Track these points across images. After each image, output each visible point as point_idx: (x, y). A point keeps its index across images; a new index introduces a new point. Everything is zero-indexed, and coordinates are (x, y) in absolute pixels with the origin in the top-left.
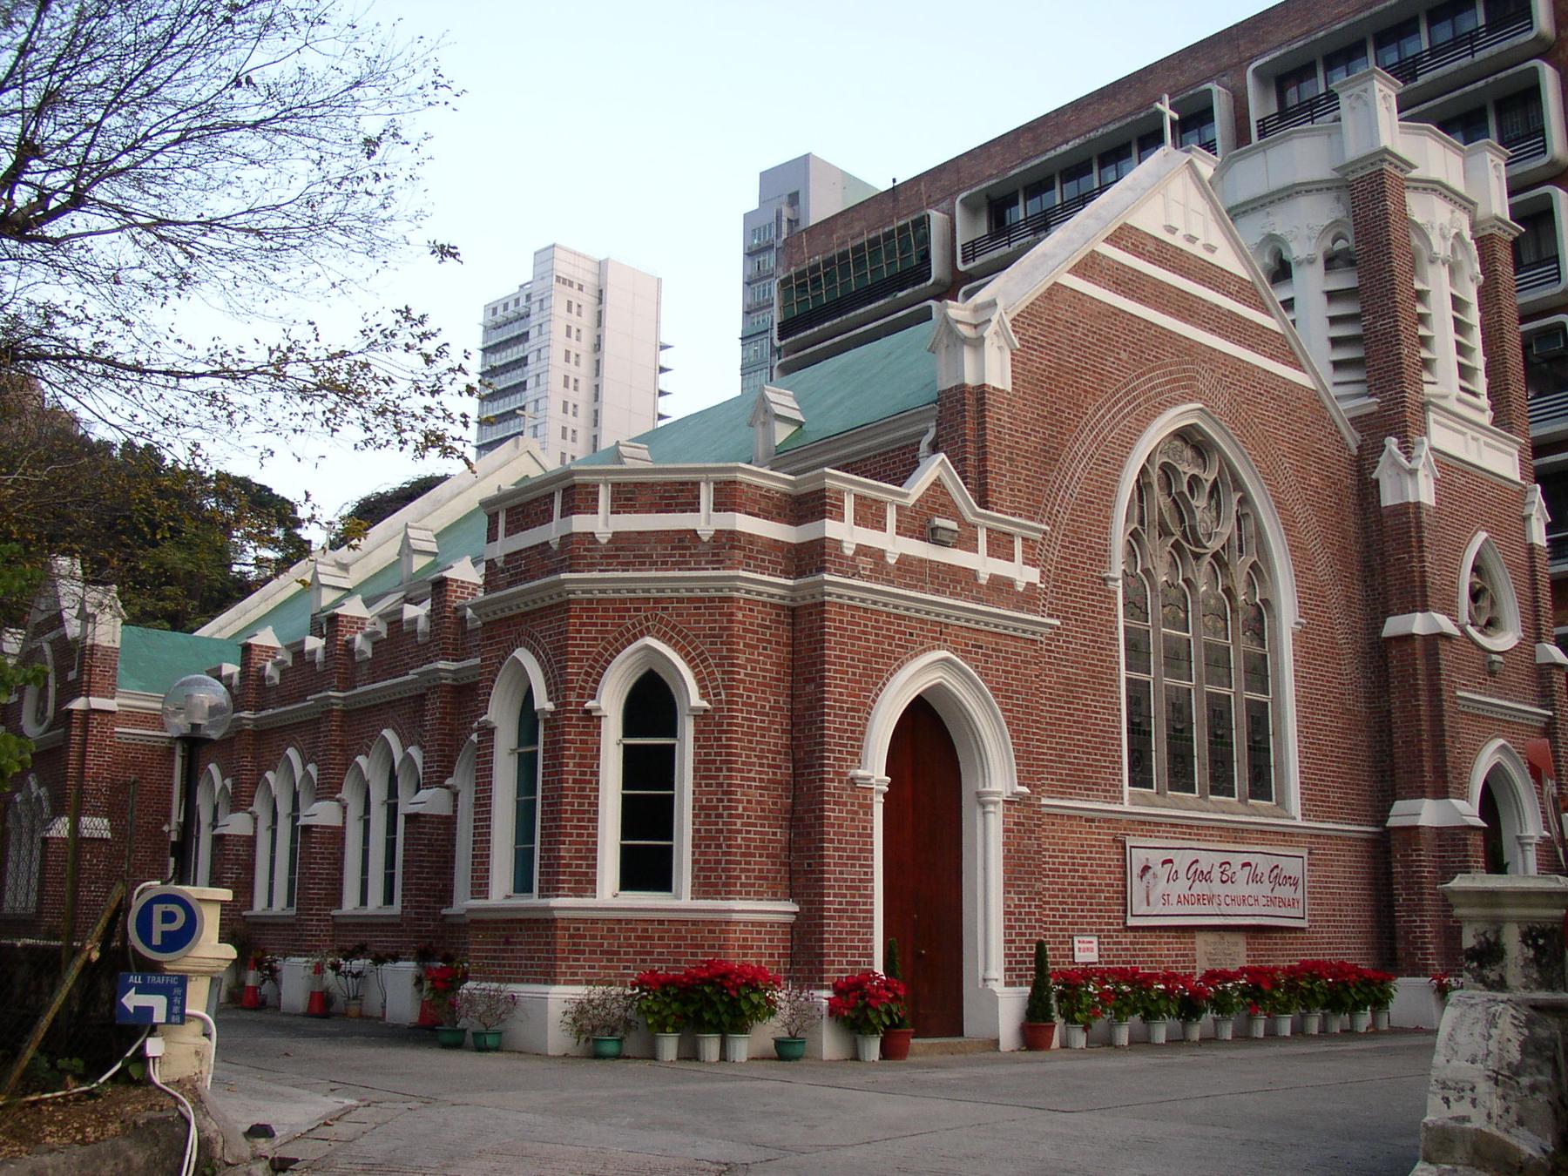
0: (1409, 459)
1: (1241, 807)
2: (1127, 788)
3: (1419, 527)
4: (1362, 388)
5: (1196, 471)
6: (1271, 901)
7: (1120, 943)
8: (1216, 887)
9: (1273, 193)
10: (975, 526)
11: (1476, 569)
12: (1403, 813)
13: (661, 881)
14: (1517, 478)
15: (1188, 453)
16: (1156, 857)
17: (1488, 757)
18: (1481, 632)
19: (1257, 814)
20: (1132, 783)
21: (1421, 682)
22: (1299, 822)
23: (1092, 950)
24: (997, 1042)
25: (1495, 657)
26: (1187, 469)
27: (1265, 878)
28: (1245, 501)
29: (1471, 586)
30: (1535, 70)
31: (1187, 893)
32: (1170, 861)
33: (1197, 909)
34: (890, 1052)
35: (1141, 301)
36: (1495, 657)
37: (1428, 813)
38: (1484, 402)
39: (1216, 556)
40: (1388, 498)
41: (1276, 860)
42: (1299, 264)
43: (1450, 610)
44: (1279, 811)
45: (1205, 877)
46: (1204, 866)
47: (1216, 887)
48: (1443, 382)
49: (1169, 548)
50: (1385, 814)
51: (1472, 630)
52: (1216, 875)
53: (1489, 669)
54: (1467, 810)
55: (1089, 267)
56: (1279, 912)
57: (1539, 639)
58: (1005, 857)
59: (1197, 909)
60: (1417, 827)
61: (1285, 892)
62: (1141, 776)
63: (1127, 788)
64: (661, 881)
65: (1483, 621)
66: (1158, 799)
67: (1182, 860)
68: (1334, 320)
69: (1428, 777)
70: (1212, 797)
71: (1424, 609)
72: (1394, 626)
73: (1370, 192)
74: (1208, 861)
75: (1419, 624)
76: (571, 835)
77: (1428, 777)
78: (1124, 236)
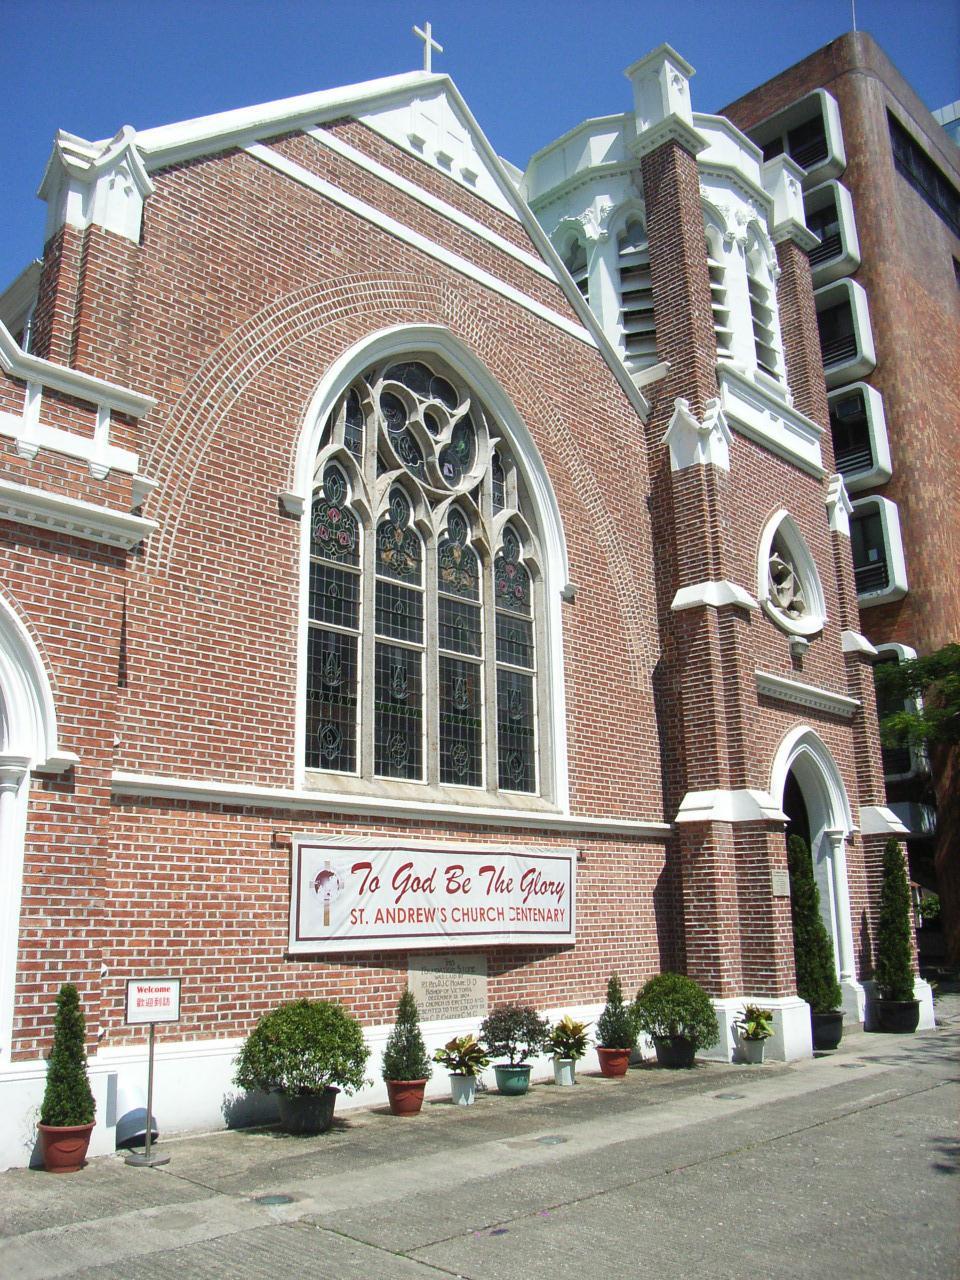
0: (700, 420)
3: (711, 492)
6: (522, 914)
8: (439, 898)
11: (778, 546)
12: (696, 806)
16: (341, 862)
18: (784, 613)
19: (516, 805)
20: (312, 760)
21: (716, 656)
22: (567, 817)
23: (166, 1002)
27: (516, 885)
29: (772, 565)
30: (817, 97)
31: (392, 906)
32: (367, 865)
33: (408, 927)
35: (369, 201)
38: (783, 384)
39: (460, 500)
41: (531, 863)
43: (747, 581)
45: (424, 885)
46: (421, 870)
47: (439, 898)
51: (776, 612)
52: (440, 882)
54: (771, 803)
56: (532, 926)
57: (844, 626)
58: (28, 858)
59: (408, 927)
61: (545, 901)
62: (329, 746)
65: (785, 602)
67: (385, 865)
69: (724, 764)
72: (684, 598)
73: (658, 172)
74: (423, 866)
76: (115, 885)
77: (724, 764)
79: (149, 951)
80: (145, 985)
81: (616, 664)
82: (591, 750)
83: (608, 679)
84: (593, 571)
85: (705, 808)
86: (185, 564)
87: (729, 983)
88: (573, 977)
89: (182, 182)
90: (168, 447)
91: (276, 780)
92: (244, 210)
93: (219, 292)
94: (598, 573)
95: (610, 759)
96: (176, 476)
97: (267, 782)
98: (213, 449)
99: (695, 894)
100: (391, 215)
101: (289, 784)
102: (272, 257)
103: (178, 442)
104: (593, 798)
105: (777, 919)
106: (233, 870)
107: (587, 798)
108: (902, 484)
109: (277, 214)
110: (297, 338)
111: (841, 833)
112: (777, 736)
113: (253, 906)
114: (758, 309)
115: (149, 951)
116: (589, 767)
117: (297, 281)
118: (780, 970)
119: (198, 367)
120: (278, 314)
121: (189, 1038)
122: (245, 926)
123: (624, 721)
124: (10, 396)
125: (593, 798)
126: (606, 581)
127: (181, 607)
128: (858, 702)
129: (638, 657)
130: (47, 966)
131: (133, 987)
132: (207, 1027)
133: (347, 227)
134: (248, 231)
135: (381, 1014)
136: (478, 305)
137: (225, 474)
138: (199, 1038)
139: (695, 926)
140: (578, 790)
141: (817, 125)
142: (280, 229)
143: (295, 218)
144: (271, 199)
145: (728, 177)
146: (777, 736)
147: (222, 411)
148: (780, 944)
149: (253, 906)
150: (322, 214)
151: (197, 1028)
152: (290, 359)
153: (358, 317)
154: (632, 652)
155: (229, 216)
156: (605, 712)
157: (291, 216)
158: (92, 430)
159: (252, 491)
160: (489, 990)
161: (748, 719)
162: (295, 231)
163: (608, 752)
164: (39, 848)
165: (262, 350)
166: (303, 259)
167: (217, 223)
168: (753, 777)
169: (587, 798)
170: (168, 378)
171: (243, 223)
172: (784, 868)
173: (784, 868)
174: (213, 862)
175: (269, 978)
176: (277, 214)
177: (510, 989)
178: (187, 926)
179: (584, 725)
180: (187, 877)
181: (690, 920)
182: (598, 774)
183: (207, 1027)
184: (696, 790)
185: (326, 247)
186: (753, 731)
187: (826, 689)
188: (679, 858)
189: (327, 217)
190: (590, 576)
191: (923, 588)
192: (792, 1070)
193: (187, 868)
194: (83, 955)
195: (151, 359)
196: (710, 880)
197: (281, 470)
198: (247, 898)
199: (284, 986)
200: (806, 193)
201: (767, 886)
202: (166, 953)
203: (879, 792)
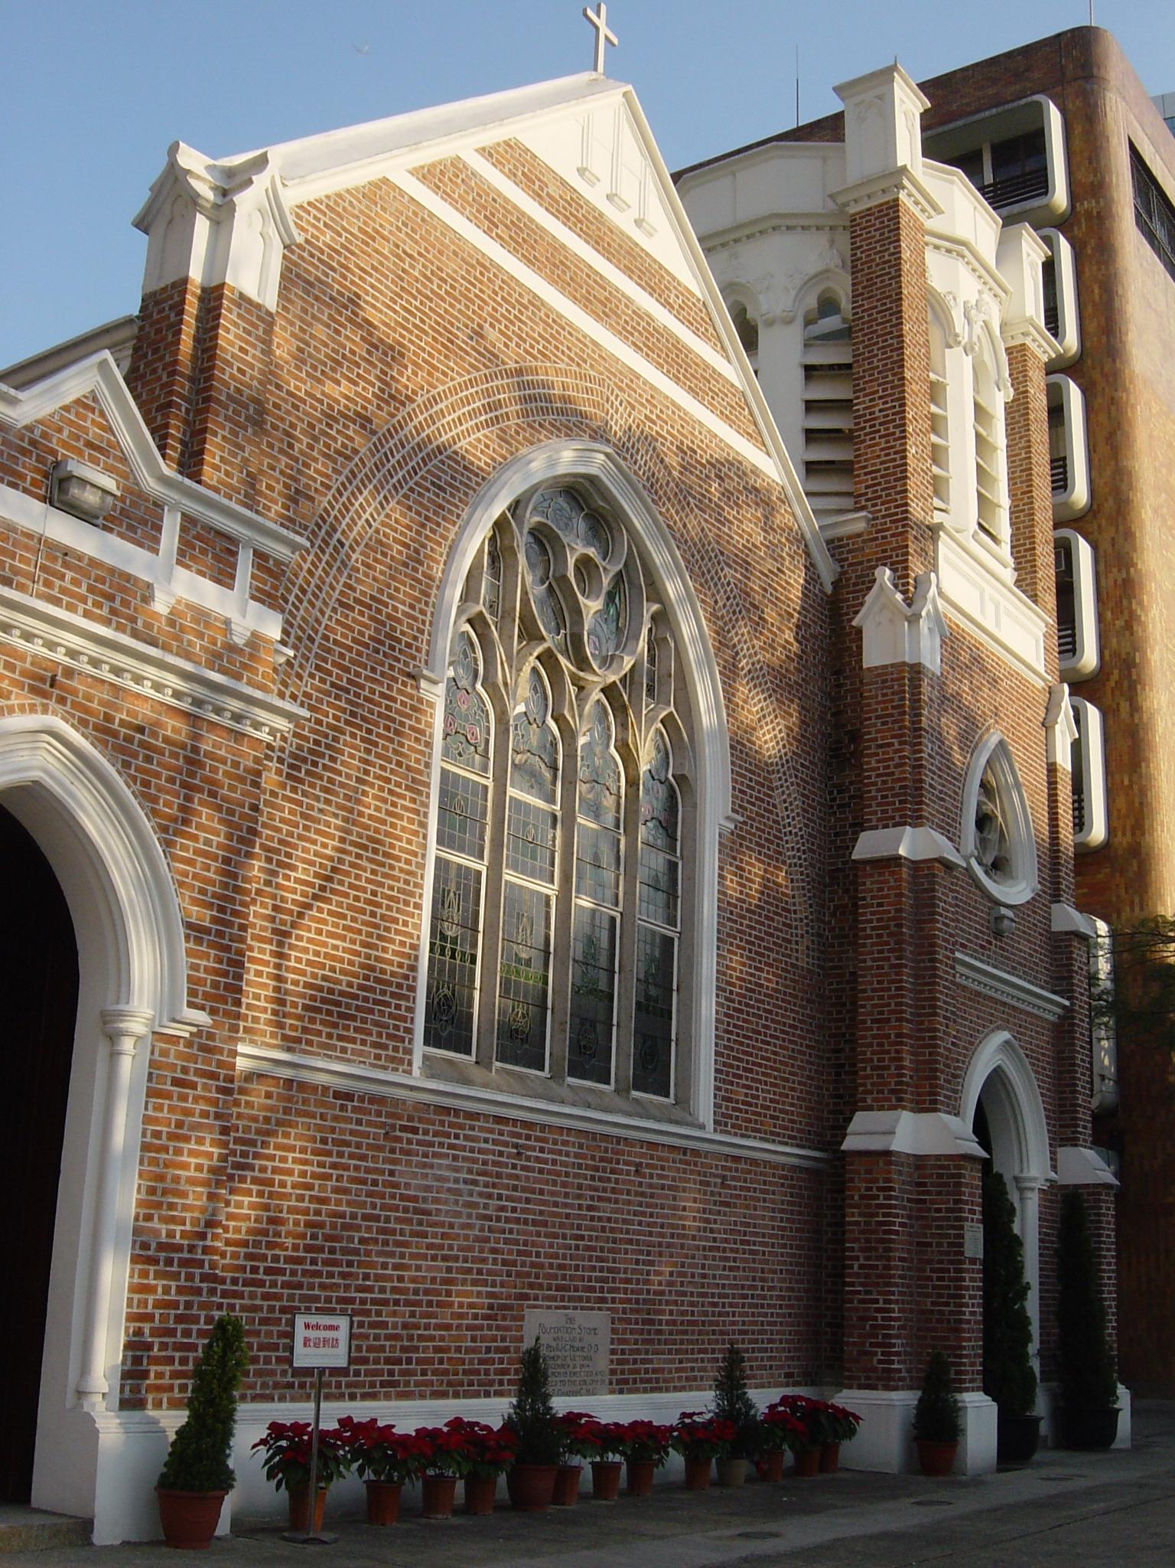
1: (619, 1102)
2: (419, 1048)
3: (916, 702)
4: (847, 503)
5: (592, 552)
7: (383, 1325)
9: (739, 227)
10: (158, 505)
12: (864, 1131)
13: (147, 1277)
14: (1041, 669)
15: (581, 525)
17: (990, 1053)
23: (335, 1343)
24: (86, 1526)
25: (1004, 911)
26: (577, 547)
28: (663, 619)
34: (374, 1421)
35: (530, 262)
36: (1004, 911)
37: (907, 1133)
38: (1005, 550)
39: (609, 690)
40: (874, 655)
42: (770, 323)
43: (950, 828)
44: (677, 1113)
48: (959, 510)
49: (532, 661)
50: (840, 1130)
51: (979, 871)
53: (995, 927)
55: (445, 177)
57: (1056, 897)
60: (887, 1153)
63: (419, 1048)
64: (147, 1277)
65: (989, 860)
66: (477, 1073)
68: (810, 406)
70: (570, 1080)
71: (917, 820)
72: (868, 845)
75: (910, 843)
78: (515, 159)
79: (244, 1280)
80: (313, 1320)
81: (776, 929)
82: (741, 1044)
83: (765, 948)
84: (757, 798)
85: (884, 1133)
86: (305, 760)
87: (899, 1371)
88: (705, 1351)
89: (321, 225)
90: (292, 598)
91: (393, 1059)
92: (388, 269)
93: (356, 384)
94: (763, 801)
95: (763, 1058)
96: (299, 639)
97: (382, 1062)
98: (342, 604)
99: (861, 1250)
100: (553, 282)
101: (405, 1067)
102: (417, 336)
103: (304, 591)
104: (740, 1110)
105: (967, 1288)
106: (339, 1178)
107: (734, 1109)
108: (1112, 684)
109: (425, 276)
110: (441, 453)
111: (1035, 1179)
112: (972, 1043)
113: (358, 1228)
114: (982, 444)
115: (244, 1280)
116: (738, 1068)
117: (445, 374)
118: (967, 1356)
119: (329, 488)
120: (421, 418)
121: (282, 1399)
122: (349, 1254)
123: (780, 1007)
124: (146, 525)
125: (740, 1110)
126: (771, 812)
127: (298, 819)
128: (1067, 1003)
129: (801, 920)
130: (160, 1290)
131: (300, 1321)
132: (302, 1386)
133: (503, 298)
134: (392, 299)
135: (491, 1383)
136: (646, 416)
137: (354, 640)
138: (293, 1400)
139: (859, 1292)
140: (724, 1099)
141: (1037, 141)
142: (427, 297)
143: (445, 282)
144: (420, 254)
145: (956, 247)
146: (972, 1043)
147: (354, 551)
148: (968, 1322)
149: (358, 1228)
150: (475, 278)
151: (291, 1385)
152: (433, 484)
153: (509, 427)
154: (795, 912)
155: (371, 276)
156: (760, 993)
157: (441, 279)
158: (233, 577)
159: (383, 665)
160: (612, 1361)
161: (945, 1017)
162: (444, 300)
163: (761, 1049)
164: (157, 1135)
165: (401, 468)
166: (452, 342)
167: (357, 286)
168: (946, 1097)
169: (734, 1109)
170: (296, 502)
171: (387, 287)
172: (978, 1221)
173: (978, 1221)
174: (319, 1165)
175: (372, 1325)
176: (425, 276)
177: (635, 1361)
178: (286, 1249)
179: (735, 1009)
180: (289, 1184)
181: (852, 1284)
182: (747, 1078)
183: (302, 1386)
184: (870, 1108)
185: (479, 325)
186: (948, 1034)
187: (1029, 982)
188: (843, 1200)
189: (481, 282)
190: (753, 804)
191: (1129, 838)
192: (983, 1483)
193: (290, 1172)
194: (197, 1279)
195: (277, 474)
196: (886, 1232)
197: (415, 638)
198: (354, 1216)
199: (388, 1337)
200: (929, 133)
201: (958, 1245)
202: (261, 1284)
203: (1085, 1127)
